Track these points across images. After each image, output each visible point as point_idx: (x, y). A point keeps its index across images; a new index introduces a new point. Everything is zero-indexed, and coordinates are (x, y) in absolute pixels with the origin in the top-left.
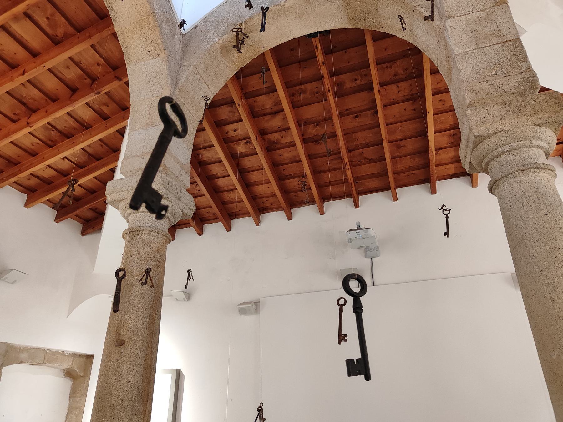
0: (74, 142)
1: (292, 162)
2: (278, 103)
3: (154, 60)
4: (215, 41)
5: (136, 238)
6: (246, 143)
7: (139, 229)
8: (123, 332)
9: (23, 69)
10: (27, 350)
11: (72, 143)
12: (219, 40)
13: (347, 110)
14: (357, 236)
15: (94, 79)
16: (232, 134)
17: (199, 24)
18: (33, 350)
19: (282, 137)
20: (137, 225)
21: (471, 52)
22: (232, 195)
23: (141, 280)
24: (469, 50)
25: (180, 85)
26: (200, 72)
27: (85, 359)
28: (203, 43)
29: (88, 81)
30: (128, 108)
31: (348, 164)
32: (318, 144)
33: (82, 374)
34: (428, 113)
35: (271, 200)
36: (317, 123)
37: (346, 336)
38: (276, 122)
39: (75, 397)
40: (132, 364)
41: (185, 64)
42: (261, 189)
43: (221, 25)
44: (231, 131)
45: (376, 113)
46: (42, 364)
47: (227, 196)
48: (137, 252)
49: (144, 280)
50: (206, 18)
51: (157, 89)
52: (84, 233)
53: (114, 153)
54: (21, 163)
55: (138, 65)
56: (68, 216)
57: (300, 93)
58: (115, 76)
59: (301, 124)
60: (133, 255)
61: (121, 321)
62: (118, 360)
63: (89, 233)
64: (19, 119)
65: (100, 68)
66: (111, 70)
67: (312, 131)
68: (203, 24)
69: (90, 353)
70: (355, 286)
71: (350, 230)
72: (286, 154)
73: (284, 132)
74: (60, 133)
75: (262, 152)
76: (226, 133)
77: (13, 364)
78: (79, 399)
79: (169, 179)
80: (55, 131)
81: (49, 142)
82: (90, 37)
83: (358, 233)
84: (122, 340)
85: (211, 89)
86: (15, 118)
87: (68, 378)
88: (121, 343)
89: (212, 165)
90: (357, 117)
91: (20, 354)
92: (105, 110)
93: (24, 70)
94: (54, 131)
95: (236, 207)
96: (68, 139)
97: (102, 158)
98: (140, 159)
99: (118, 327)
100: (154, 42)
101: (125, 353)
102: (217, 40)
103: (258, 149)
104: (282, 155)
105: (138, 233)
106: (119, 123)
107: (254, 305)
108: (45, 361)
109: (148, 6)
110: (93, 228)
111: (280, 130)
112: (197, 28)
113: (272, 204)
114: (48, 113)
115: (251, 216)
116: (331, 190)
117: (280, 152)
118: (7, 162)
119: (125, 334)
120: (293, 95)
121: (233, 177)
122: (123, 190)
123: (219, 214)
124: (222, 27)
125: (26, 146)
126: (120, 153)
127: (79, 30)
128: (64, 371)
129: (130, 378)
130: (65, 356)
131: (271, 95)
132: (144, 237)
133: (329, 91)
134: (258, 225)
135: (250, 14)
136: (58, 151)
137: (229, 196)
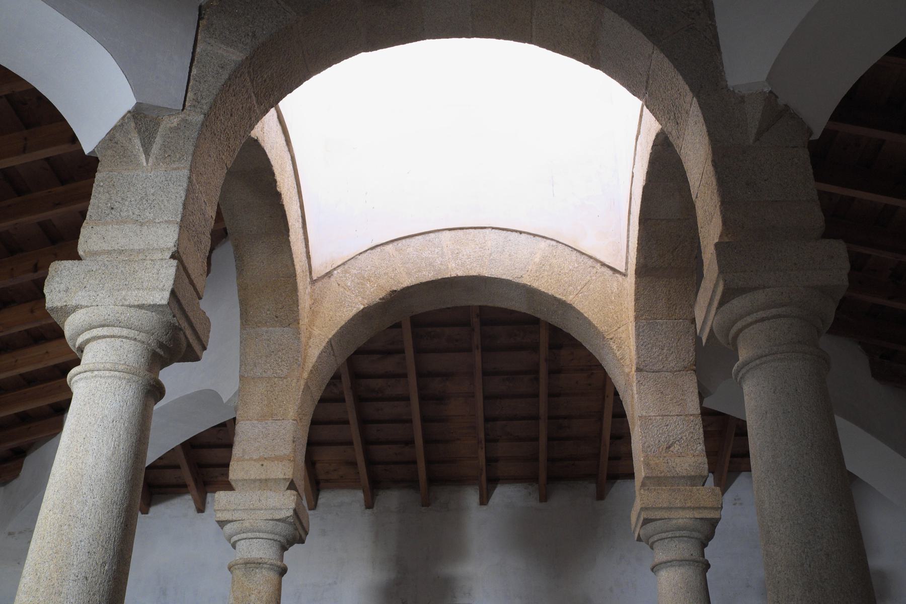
5: (254, 571)
7: (260, 561)
21: (654, 418)
24: (652, 414)
34: (607, 397)
45: (537, 379)
48: (256, 591)
55: (257, 329)
60: (252, 593)
98: (258, 465)
105: (258, 566)
122: (239, 507)
135: (408, 281)
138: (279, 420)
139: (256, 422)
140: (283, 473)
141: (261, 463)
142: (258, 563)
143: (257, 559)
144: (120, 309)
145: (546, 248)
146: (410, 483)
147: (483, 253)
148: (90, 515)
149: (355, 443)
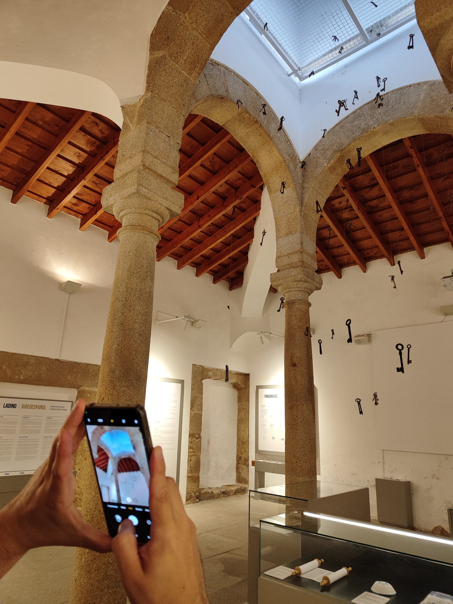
0: (225, 231)
1: (391, 220)
2: (374, 179)
3: (287, 189)
4: (324, 166)
6: (351, 210)
7: (293, 301)
8: (294, 359)
9: (197, 195)
10: (211, 370)
11: (224, 232)
12: (327, 165)
13: (437, 174)
14: (450, 282)
15: (236, 189)
16: (337, 205)
17: (312, 152)
18: (214, 371)
19: (381, 202)
20: (291, 299)
22: (340, 250)
23: (305, 334)
25: (305, 203)
26: (316, 189)
27: (244, 376)
28: (316, 168)
29: (233, 191)
30: (258, 201)
31: (443, 217)
32: (413, 203)
33: (243, 387)
35: (375, 251)
36: (410, 187)
37: (411, 361)
38: (374, 192)
39: (241, 402)
40: (302, 376)
41: (306, 186)
42: (365, 243)
43: (328, 152)
44: (337, 204)
46: (221, 379)
47: (336, 252)
49: (306, 334)
50: (316, 147)
51: (291, 208)
52: (231, 288)
53: (249, 232)
54: (192, 249)
56: (222, 278)
57: (394, 169)
58: (251, 185)
59: (395, 191)
61: (292, 353)
62: (294, 374)
63: (234, 289)
64: (193, 223)
65: (240, 181)
66: (247, 180)
67: (406, 194)
68: (314, 152)
69: (247, 372)
70: (400, 347)
71: (444, 278)
72: (385, 215)
73: (382, 199)
74: (216, 227)
75: (364, 217)
76: (333, 206)
77: (206, 379)
78: (244, 403)
79: (307, 269)
80: (213, 226)
81: (209, 233)
82: (236, 167)
83: (451, 280)
84: (294, 364)
85: (324, 196)
86: (189, 223)
87: (235, 389)
88: (294, 365)
89: (323, 230)
90: (448, 178)
91: (209, 373)
92: (243, 205)
93: (198, 195)
94: (212, 226)
95: (345, 259)
96: (221, 229)
97: (241, 237)
98: (287, 258)
99: (291, 356)
100: (286, 178)
101: (297, 370)
102: (326, 165)
103: (360, 215)
104: (382, 216)
105: (293, 304)
106: (254, 214)
107: (367, 337)
108: (222, 377)
109: (280, 158)
110: (237, 284)
111: (378, 198)
112: (311, 156)
113: (376, 254)
114: (211, 217)
115: (357, 265)
116: (428, 238)
117: (380, 213)
118: (185, 250)
119: (295, 360)
120: (387, 171)
121: (340, 238)
123: (330, 266)
124: (329, 153)
125: (196, 238)
126: (254, 232)
127: (228, 162)
128: (232, 384)
129: (302, 383)
130: (232, 374)
131: (368, 174)
132: (297, 306)
133: (418, 166)
134: (365, 272)
136: (216, 238)
137: (338, 251)
138: (294, 234)
139: (284, 238)
140: (298, 259)
141: (288, 256)
142: (292, 303)
143: (292, 301)
144: (123, 201)
145: (427, 88)
146: (410, 248)
147: (388, 108)
148: (121, 296)
149: (373, 237)
